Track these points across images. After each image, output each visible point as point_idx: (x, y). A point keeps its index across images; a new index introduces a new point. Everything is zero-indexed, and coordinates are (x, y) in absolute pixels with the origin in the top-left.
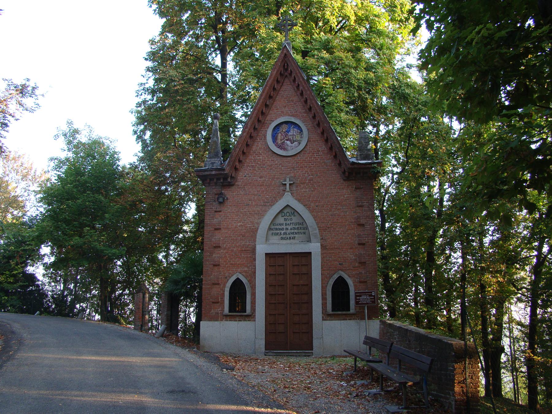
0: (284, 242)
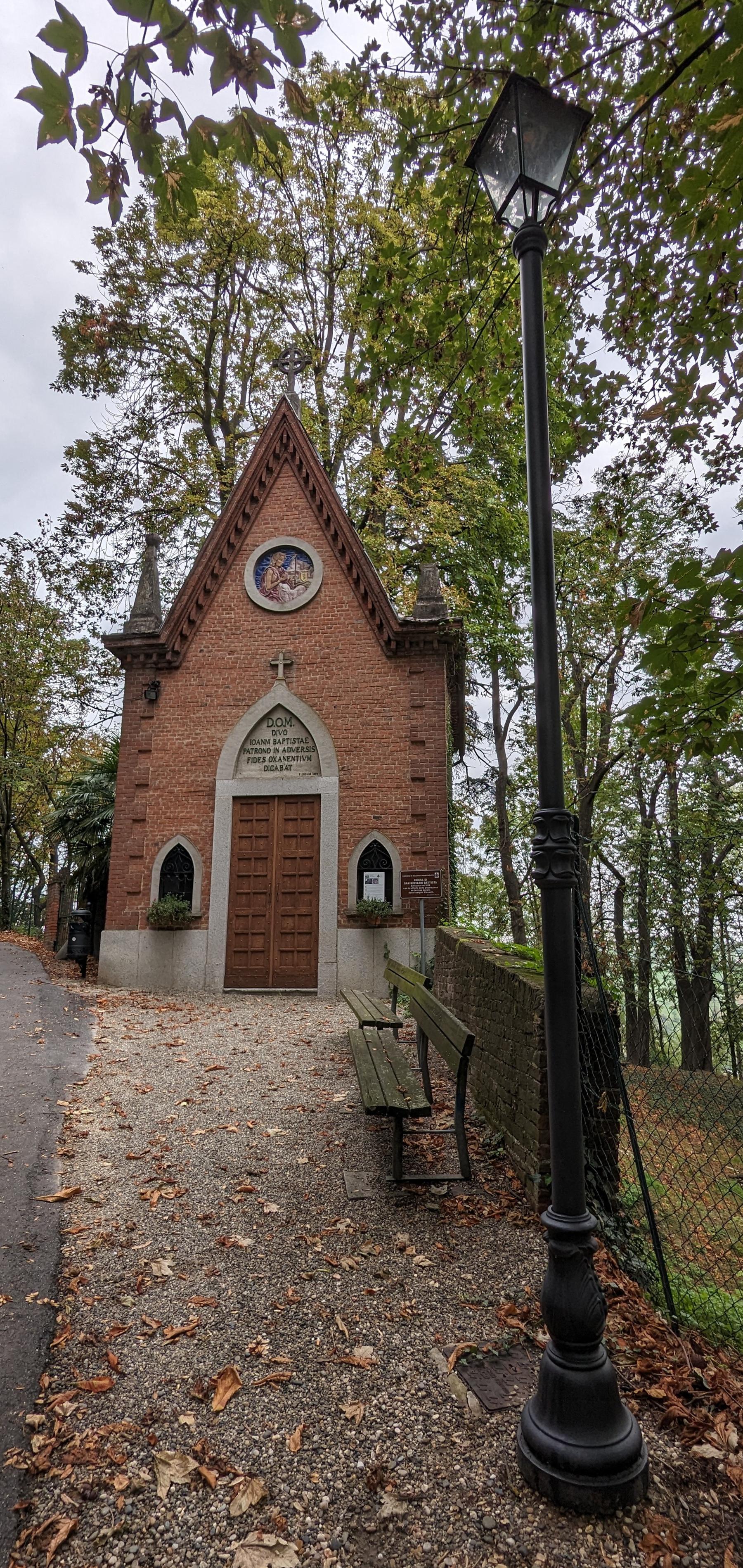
0: (270, 775)
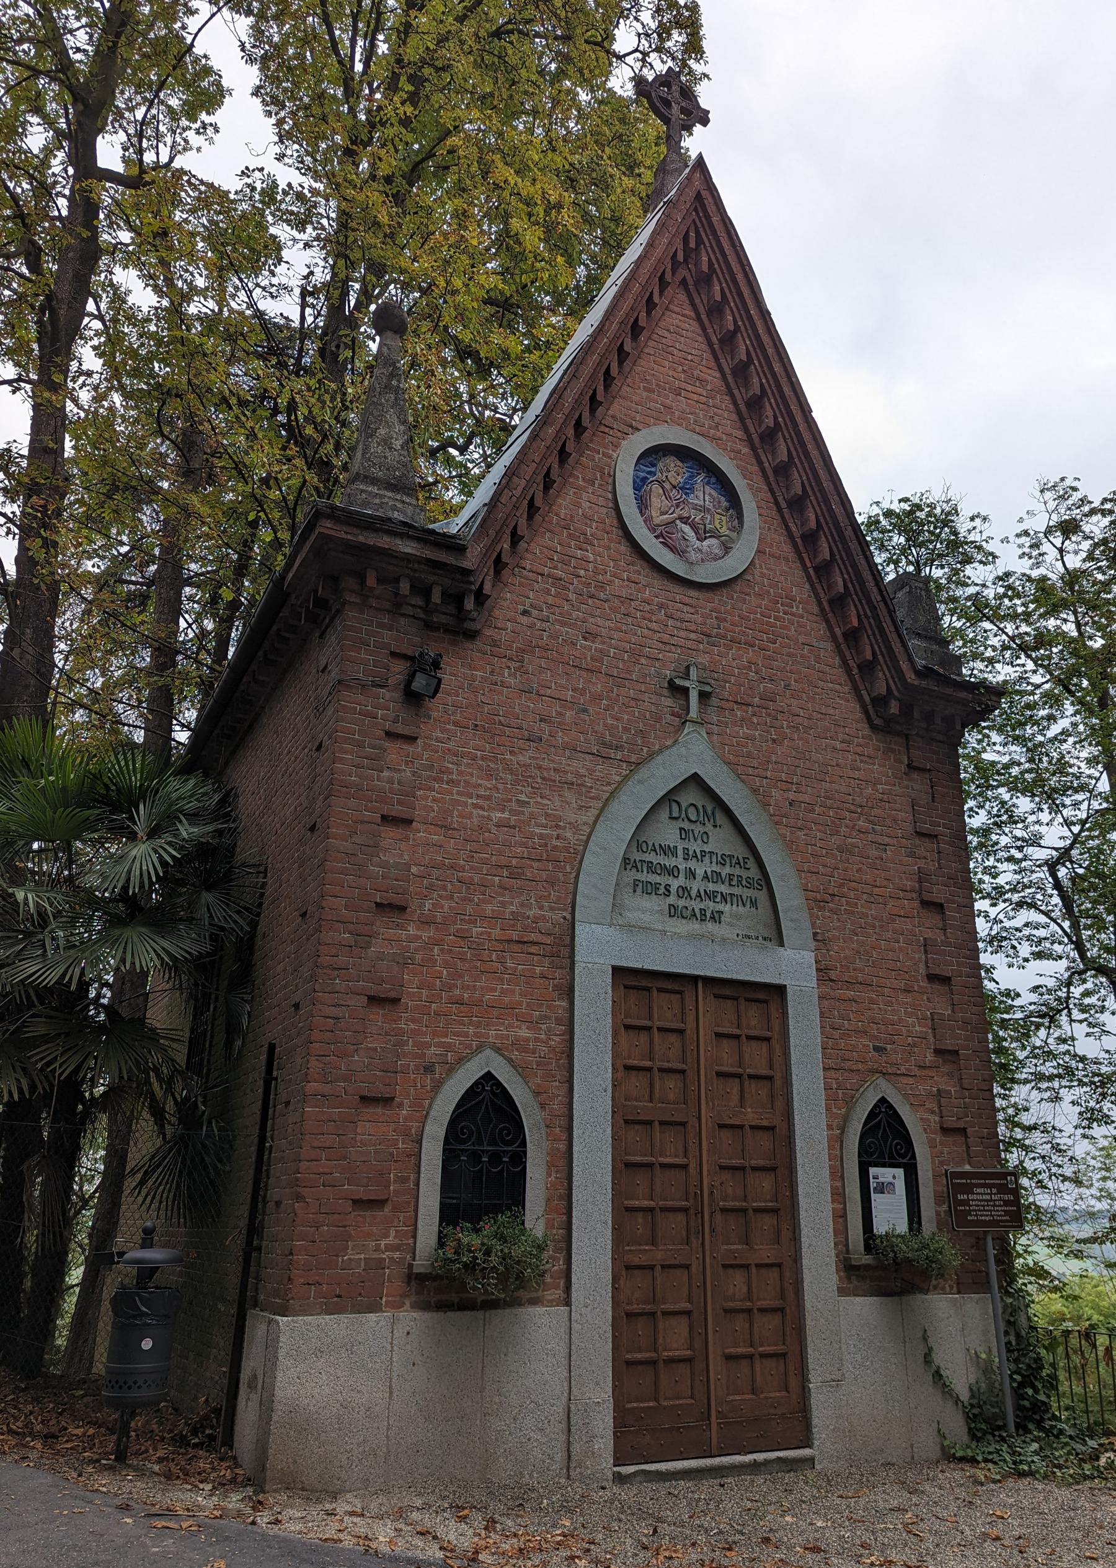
0: (682, 927)
